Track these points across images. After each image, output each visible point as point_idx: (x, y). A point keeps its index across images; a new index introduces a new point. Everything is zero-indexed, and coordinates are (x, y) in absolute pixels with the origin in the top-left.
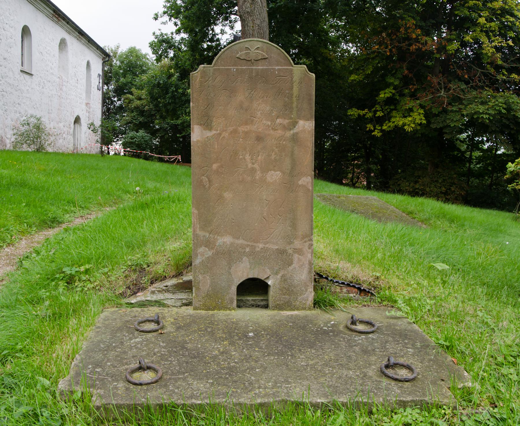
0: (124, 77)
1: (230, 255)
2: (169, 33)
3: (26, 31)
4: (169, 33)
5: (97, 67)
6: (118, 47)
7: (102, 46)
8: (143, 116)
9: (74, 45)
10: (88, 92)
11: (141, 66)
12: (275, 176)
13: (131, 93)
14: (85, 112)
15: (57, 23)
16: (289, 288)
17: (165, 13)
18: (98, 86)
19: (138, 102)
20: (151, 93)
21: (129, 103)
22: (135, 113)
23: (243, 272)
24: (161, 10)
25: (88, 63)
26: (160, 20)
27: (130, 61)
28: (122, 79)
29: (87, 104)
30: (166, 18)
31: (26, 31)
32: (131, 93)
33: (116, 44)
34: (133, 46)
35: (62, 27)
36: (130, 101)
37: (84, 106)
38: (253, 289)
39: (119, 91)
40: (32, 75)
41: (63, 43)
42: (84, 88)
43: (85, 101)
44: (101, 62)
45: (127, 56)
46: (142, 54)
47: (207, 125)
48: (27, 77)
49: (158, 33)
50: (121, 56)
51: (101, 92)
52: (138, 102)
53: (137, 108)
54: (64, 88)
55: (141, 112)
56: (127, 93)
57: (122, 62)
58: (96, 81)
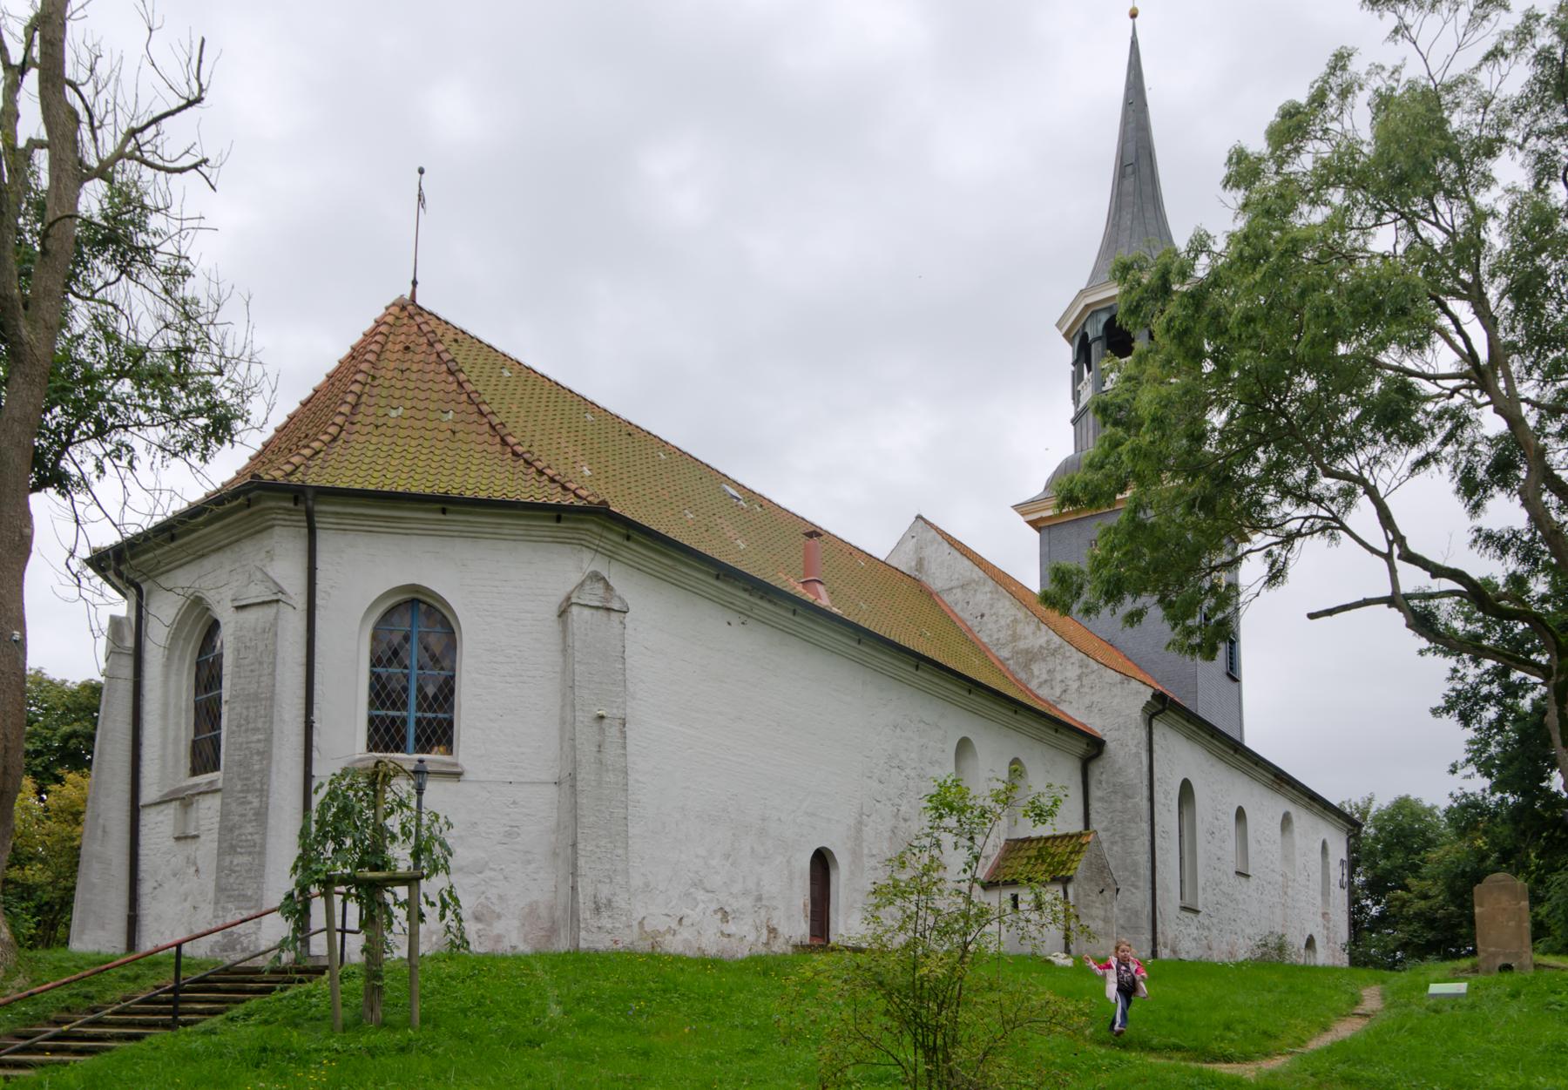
0: (1388, 857)
1: (1495, 955)
2: (1478, 791)
3: (1240, 814)
4: (1478, 791)
5: (1339, 850)
6: (1370, 800)
7: (1335, 803)
8: (1433, 929)
9: (1304, 820)
10: (1325, 893)
11: (1423, 832)
12: (1512, 924)
13: (1406, 888)
14: (1320, 929)
15: (1277, 791)
16: (1522, 967)
17: (1468, 761)
18: (1341, 882)
19: (1422, 904)
20: (1450, 888)
21: (1403, 906)
22: (1416, 925)
23: (1501, 961)
24: (1462, 757)
25: (1324, 844)
26: (1461, 773)
27: (1398, 825)
28: (1382, 863)
29: (1324, 915)
30: (1472, 769)
31: (1240, 814)
32: (1406, 888)
33: (1367, 795)
34: (1403, 794)
35: (1284, 795)
36: (1404, 903)
37: (1319, 919)
38: (1507, 968)
39: (1377, 887)
40: (1248, 876)
41: (1286, 820)
42: (1318, 888)
43: (1320, 911)
44: (1344, 837)
45: (1392, 817)
46: (1423, 809)
47: (1481, 906)
48: (1243, 879)
49: (1458, 793)
50: (1375, 819)
51: (1345, 892)
52: (1422, 904)
53: (1419, 915)
54: (1290, 891)
55: (1429, 921)
56: (1393, 888)
57: (1380, 829)
58: (1337, 873)
